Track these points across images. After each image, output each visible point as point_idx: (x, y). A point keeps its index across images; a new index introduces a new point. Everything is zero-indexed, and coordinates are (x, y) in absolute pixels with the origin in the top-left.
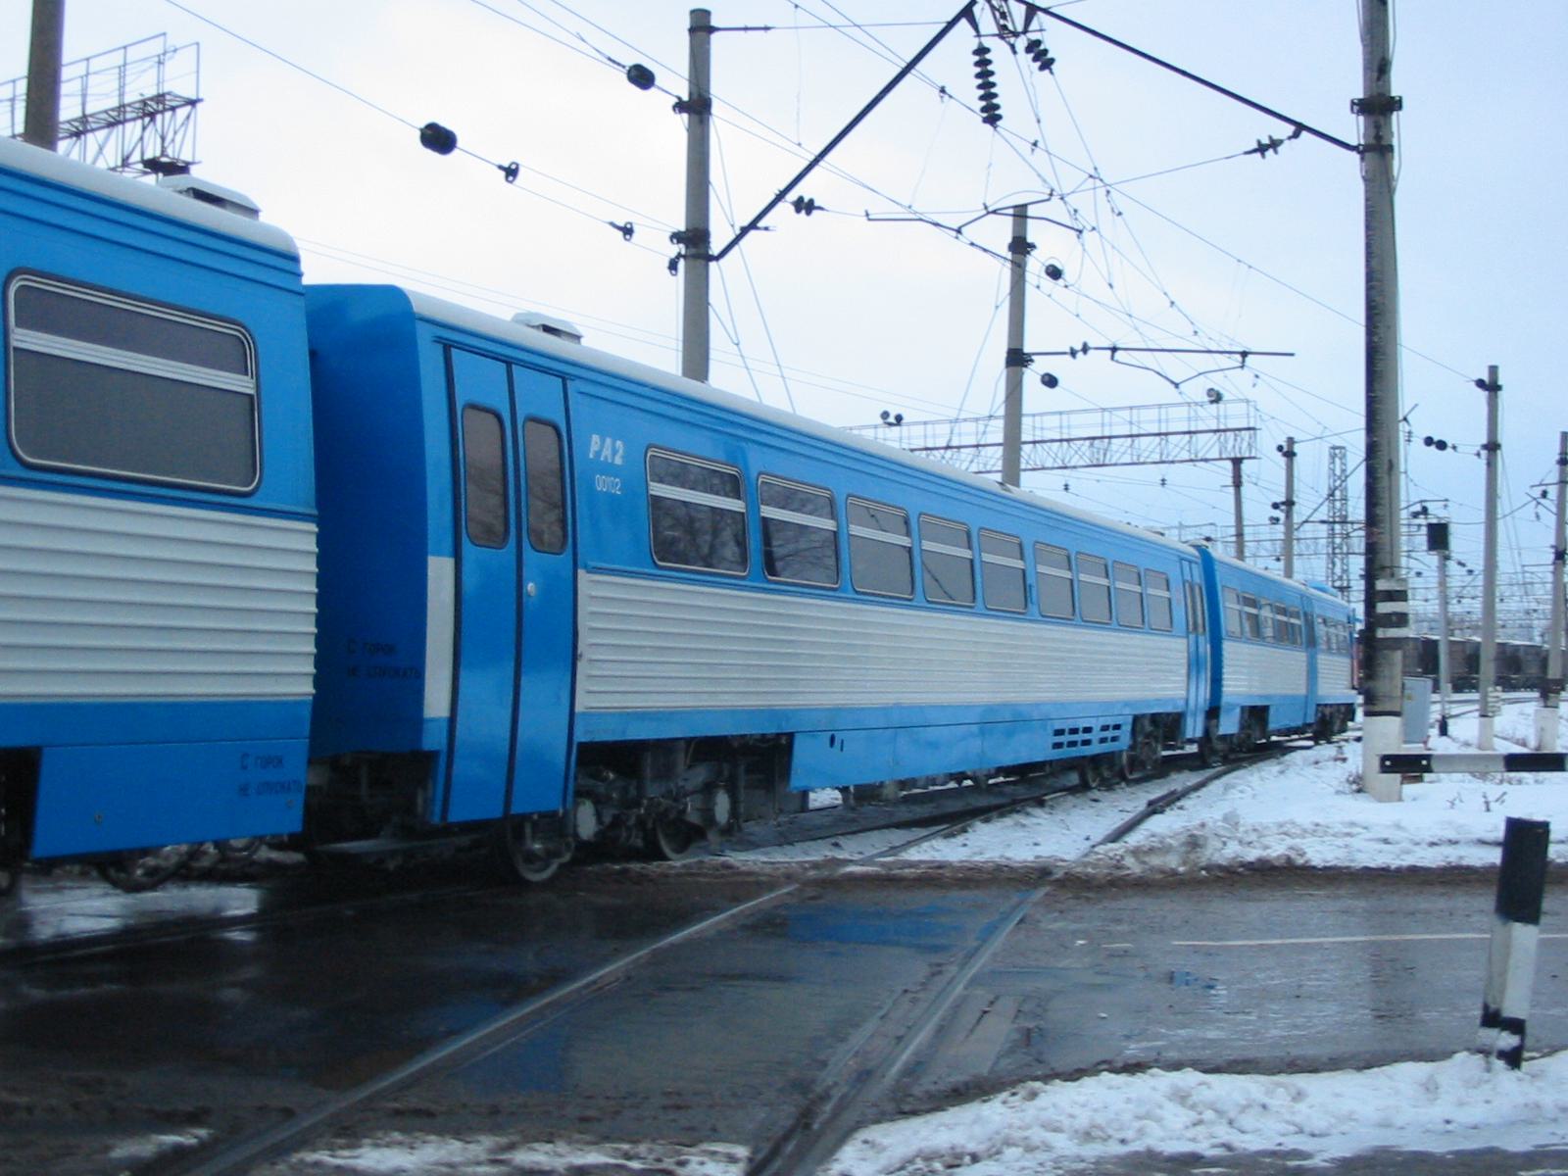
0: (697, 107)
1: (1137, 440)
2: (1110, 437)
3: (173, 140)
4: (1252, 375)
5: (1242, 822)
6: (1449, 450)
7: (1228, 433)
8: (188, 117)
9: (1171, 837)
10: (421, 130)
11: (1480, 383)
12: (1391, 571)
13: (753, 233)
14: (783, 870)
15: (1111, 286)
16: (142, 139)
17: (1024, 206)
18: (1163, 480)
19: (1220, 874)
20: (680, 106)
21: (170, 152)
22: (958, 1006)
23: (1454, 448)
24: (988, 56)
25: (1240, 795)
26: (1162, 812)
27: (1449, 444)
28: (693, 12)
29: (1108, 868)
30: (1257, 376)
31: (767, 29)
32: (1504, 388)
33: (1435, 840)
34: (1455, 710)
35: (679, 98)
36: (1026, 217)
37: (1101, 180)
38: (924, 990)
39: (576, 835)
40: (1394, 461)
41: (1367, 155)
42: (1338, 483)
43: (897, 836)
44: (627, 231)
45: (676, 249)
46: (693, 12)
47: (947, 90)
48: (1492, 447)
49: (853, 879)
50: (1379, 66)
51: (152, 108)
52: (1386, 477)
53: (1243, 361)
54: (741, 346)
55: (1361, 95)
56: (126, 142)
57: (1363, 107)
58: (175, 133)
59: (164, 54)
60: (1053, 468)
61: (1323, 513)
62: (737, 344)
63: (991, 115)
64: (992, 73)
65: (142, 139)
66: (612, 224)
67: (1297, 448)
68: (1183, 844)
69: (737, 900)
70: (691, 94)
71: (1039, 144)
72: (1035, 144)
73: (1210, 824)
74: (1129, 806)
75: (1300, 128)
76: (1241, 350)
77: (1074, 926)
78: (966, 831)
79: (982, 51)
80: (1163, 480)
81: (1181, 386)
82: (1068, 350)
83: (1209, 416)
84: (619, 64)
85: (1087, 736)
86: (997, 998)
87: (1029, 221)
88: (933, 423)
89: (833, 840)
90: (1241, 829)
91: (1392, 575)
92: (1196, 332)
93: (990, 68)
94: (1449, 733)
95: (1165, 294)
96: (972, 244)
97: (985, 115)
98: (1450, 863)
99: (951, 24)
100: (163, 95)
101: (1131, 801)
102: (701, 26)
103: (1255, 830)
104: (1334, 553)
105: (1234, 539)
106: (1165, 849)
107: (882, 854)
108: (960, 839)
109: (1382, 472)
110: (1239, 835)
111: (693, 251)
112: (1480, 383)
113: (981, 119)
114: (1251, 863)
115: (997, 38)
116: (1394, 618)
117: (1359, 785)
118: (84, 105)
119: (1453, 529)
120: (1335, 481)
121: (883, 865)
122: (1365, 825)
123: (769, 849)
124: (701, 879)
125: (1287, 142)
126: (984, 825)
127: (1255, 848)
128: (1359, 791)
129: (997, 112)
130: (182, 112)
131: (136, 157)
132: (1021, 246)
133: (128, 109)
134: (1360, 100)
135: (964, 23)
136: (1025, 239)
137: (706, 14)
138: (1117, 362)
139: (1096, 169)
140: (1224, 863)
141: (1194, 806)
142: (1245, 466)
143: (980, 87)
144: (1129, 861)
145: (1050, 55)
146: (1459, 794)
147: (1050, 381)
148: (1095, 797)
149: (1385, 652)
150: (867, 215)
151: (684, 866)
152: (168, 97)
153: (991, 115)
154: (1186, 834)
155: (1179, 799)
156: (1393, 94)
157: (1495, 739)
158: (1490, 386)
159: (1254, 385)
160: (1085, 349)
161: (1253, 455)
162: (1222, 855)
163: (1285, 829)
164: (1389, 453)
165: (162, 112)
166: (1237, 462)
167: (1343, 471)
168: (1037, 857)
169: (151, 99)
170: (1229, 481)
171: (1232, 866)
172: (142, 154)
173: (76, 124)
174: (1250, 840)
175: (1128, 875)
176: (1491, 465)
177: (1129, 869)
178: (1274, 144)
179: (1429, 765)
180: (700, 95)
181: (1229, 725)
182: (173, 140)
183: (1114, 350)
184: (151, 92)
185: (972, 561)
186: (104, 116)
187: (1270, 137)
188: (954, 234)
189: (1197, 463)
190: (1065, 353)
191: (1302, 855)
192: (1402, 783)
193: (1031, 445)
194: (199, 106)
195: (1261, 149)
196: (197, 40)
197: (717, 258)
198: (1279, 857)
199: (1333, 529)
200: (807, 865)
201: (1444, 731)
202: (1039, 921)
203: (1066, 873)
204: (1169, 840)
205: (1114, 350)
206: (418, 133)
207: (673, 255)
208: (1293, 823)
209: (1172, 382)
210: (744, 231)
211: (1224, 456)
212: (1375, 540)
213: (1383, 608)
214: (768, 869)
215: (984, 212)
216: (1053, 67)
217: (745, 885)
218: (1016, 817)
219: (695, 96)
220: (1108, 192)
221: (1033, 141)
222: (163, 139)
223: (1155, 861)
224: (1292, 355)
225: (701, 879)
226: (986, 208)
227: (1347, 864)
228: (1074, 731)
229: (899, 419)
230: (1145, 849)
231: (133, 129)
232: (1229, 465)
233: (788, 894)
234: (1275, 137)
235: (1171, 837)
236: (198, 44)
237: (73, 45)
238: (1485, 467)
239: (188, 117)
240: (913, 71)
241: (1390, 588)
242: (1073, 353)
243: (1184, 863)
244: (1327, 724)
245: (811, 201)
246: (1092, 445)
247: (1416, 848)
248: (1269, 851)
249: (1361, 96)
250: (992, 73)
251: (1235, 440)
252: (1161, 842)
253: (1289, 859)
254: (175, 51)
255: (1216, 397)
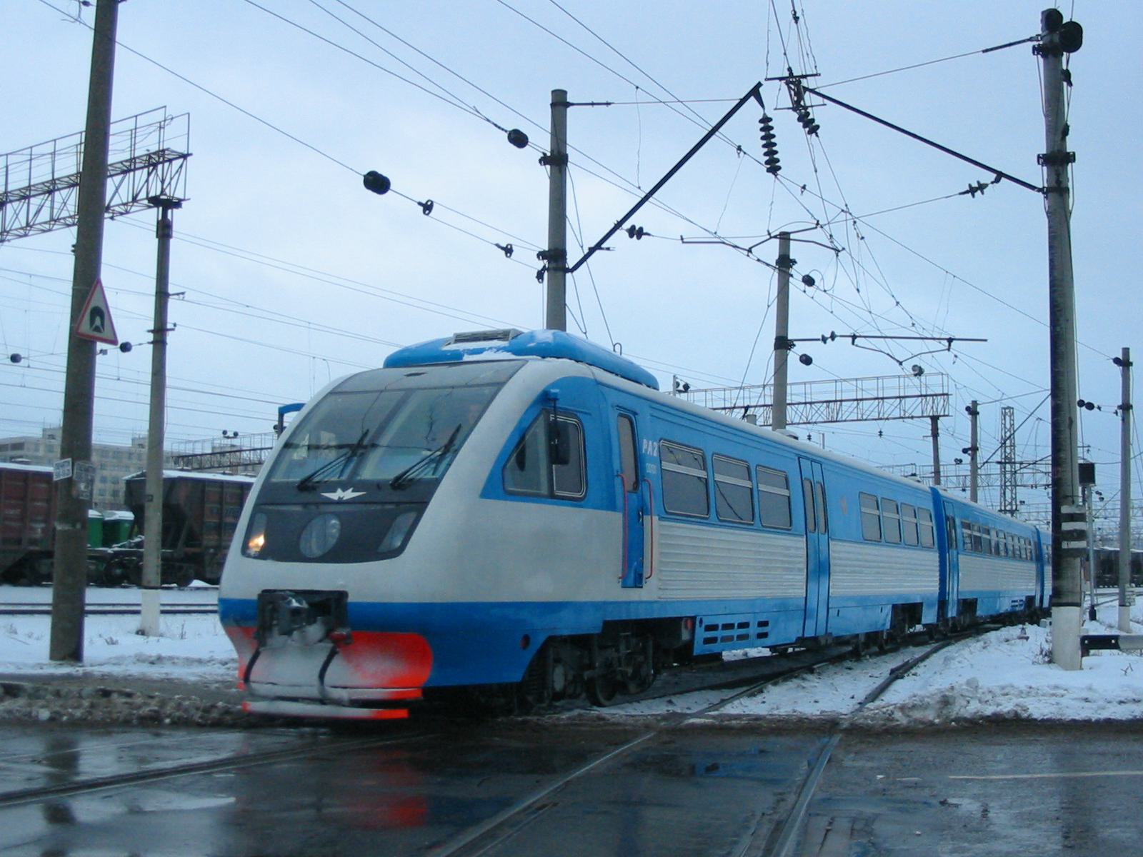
0: (557, 160)
1: (861, 403)
2: (841, 401)
3: (170, 183)
4: (953, 356)
5: (980, 685)
6: (1096, 409)
7: (928, 398)
8: (181, 167)
9: (928, 697)
10: (365, 176)
11: (1117, 361)
12: (1072, 499)
13: (598, 252)
14: (642, 721)
15: (858, 290)
16: (147, 181)
17: (788, 234)
18: (881, 432)
19: (966, 725)
20: (544, 160)
21: (167, 191)
22: (806, 825)
23: (1099, 408)
24: (770, 124)
25: (960, 665)
26: (902, 678)
27: (1096, 405)
28: (553, 92)
29: (882, 720)
30: (956, 356)
31: (608, 104)
32: (1134, 364)
33: (1123, 699)
34: (1101, 600)
35: (545, 154)
36: (790, 239)
37: (850, 214)
38: (775, 813)
39: (553, 688)
40: (1073, 417)
41: (1050, 195)
42: (1008, 434)
43: (714, 696)
44: (508, 251)
45: (541, 264)
46: (553, 92)
47: (742, 148)
48: (1126, 407)
49: (693, 727)
50: (1058, 128)
51: (156, 160)
52: (1068, 431)
53: (950, 345)
54: (587, 334)
55: (1044, 152)
56: (135, 188)
57: (1045, 160)
58: (171, 179)
59: (165, 121)
60: (799, 424)
61: (997, 457)
62: (585, 333)
63: (773, 166)
64: (774, 136)
65: (147, 181)
66: (498, 245)
67: (979, 409)
68: (938, 702)
69: (617, 744)
70: (552, 152)
71: (807, 187)
72: (804, 187)
73: (957, 687)
74: (876, 673)
75: (1000, 175)
76: (948, 337)
77: (870, 764)
78: (762, 692)
79: (765, 120)
80: (881, 432)
81: (903, 363)
82: (820, 337)
83: (913, 386)
84: (503, 129)
85: (743, 631)
86: (833, 819)
87: (791, 242)
88: (712, 390)
89: (668, 699)
90: (980, 691)
91: (1073, 502)
92: (913, 325)
93: (772, 132)
94: (1097, 618)
95: (893, 296)
96: (759, 260)
97: (768, 166)
98: (1135, 716)
99: (742, 101)
100: (163, 151)
101: (882, 667)
102: (560, 102)
103: (990, 692)
104: (1005, 486)
105: (933, 475)
106: (924, 706)
107: (709, 709)
108: (759, 698)
109: (1065, 427)
110: (979, 695)
111: (553, 265)
112: (1117, 361)
113: (766, 169)
114: (988, 716)
115: (791, 110)
116: (1075, 534)
117: (1050, 657)
118: (53, 173)
119: (1097, 468)
120: (1005, 433)
121: (714, 717)
122: (1065, 687)
123: (623, 705)
124: (583, 728)
125: (990, 185)
126: (773, 687)
127: (990, 705)
128: (1050, 662)
129: (777, 164)
130: (176, 164)
131: (142, 195)
132: (785, 263)
133: (137, 161)
134: (1043, 155)
135: (752, 99)
136: (789, 256)
137: (565, 93)
138: (857, 346)
139: (846, 205)
140: (969, 717)
141: (924, 673)
142: (941, 422)
143: (764, 146)
144: (898, 715)
145: (816, 123)
146: (1130, 664)
147: (806, 360)
148: (849, 666)
149: (1069, 559)
150: (682, 239)
151: (569, 718)
152: (167, 152)
153: (773, 166)
154: (939, 695)
155: (912, 668)
156: (1068, 151)
157: (1131, 623)
158: (1124, 363)
159: (954, 363)
160: (833, 336)
161: (946, 413)
162: (967, 711)
163: (1006, 691)
164: (1070, 411)
165: (163, 163)
166: (935, 419)
167: (1012, 425)
168: (822, 712)
169: (154, 153)
170: (930, 433)
171: (974, 719)
172: (148, 193)
173: (48, 185)
174: (986, 699)
175: (898, 725)
176: (1125, 421)
177: (897, 721)
178: (982, 187)
179: (1117, 642)
180: (559, 152)
181: (952, 612)
182: (170, 183)
183: (854, 337)
184: (154, 148)
185: (751, 490)
186: (120, 165)
187: (978, 182)
188: (746, 253)
189: (905, 420)
190: (819, 340)
191: (1026, 710)
192: (1082, 656)
193: (803, 406)
194: (189, 158)
195: (972, 191)
196: (189, 111)
197: (572, 270)
198: (1009, 712)
199: (1005, 468)
200: (659, 718)
201: (1093, 616)
202: (842, 761)
203: (852, 724)
204: (926, 699)
205: (854, 337)
206: (363, 178)
207: (540, 267)
208: (1012, 686)
209: (898, 361)
210: (592, 251)
211: (925, 415)
212: (1059, 476)
213: (1067, 526)
214: (631, 721)
215: (768, 237)
216: (818, 131)
217: (618, 734)
218: (796, 681)
219: (555, 152)
220: (855, 222)
221: (802, 185)
222: (163, 182)
223: (917, 715)
224: (986, 340)
225: (583, 728)
226: (769, 234)
227: (1059, 717)
228: (729, 626)
229: (686, 387)
230: (910, 706)
231: (141, 175)
232: (929, 420)
233: (649, 739)
234: (982, 182)
235: (928, 697)
236: (189, 114)
237: (119, 107)
238: (1120, 422)
239: (181, 167)
240: (717, 133)
241: (1072, 512)
242: (824, 340)
243: (939, 717)
244: (1032, 613)
245: (641, 229)
246: (828, 407)
247: (1109, 705)
248: (1000, 707)
249: (1045, 152)
250: (774, 136)
251: (933, 402)
252: (921, 701)
253: (1016, 712)
254: (172, 119)
255: (919, 372)
